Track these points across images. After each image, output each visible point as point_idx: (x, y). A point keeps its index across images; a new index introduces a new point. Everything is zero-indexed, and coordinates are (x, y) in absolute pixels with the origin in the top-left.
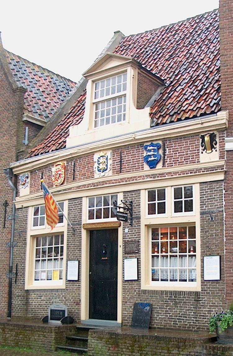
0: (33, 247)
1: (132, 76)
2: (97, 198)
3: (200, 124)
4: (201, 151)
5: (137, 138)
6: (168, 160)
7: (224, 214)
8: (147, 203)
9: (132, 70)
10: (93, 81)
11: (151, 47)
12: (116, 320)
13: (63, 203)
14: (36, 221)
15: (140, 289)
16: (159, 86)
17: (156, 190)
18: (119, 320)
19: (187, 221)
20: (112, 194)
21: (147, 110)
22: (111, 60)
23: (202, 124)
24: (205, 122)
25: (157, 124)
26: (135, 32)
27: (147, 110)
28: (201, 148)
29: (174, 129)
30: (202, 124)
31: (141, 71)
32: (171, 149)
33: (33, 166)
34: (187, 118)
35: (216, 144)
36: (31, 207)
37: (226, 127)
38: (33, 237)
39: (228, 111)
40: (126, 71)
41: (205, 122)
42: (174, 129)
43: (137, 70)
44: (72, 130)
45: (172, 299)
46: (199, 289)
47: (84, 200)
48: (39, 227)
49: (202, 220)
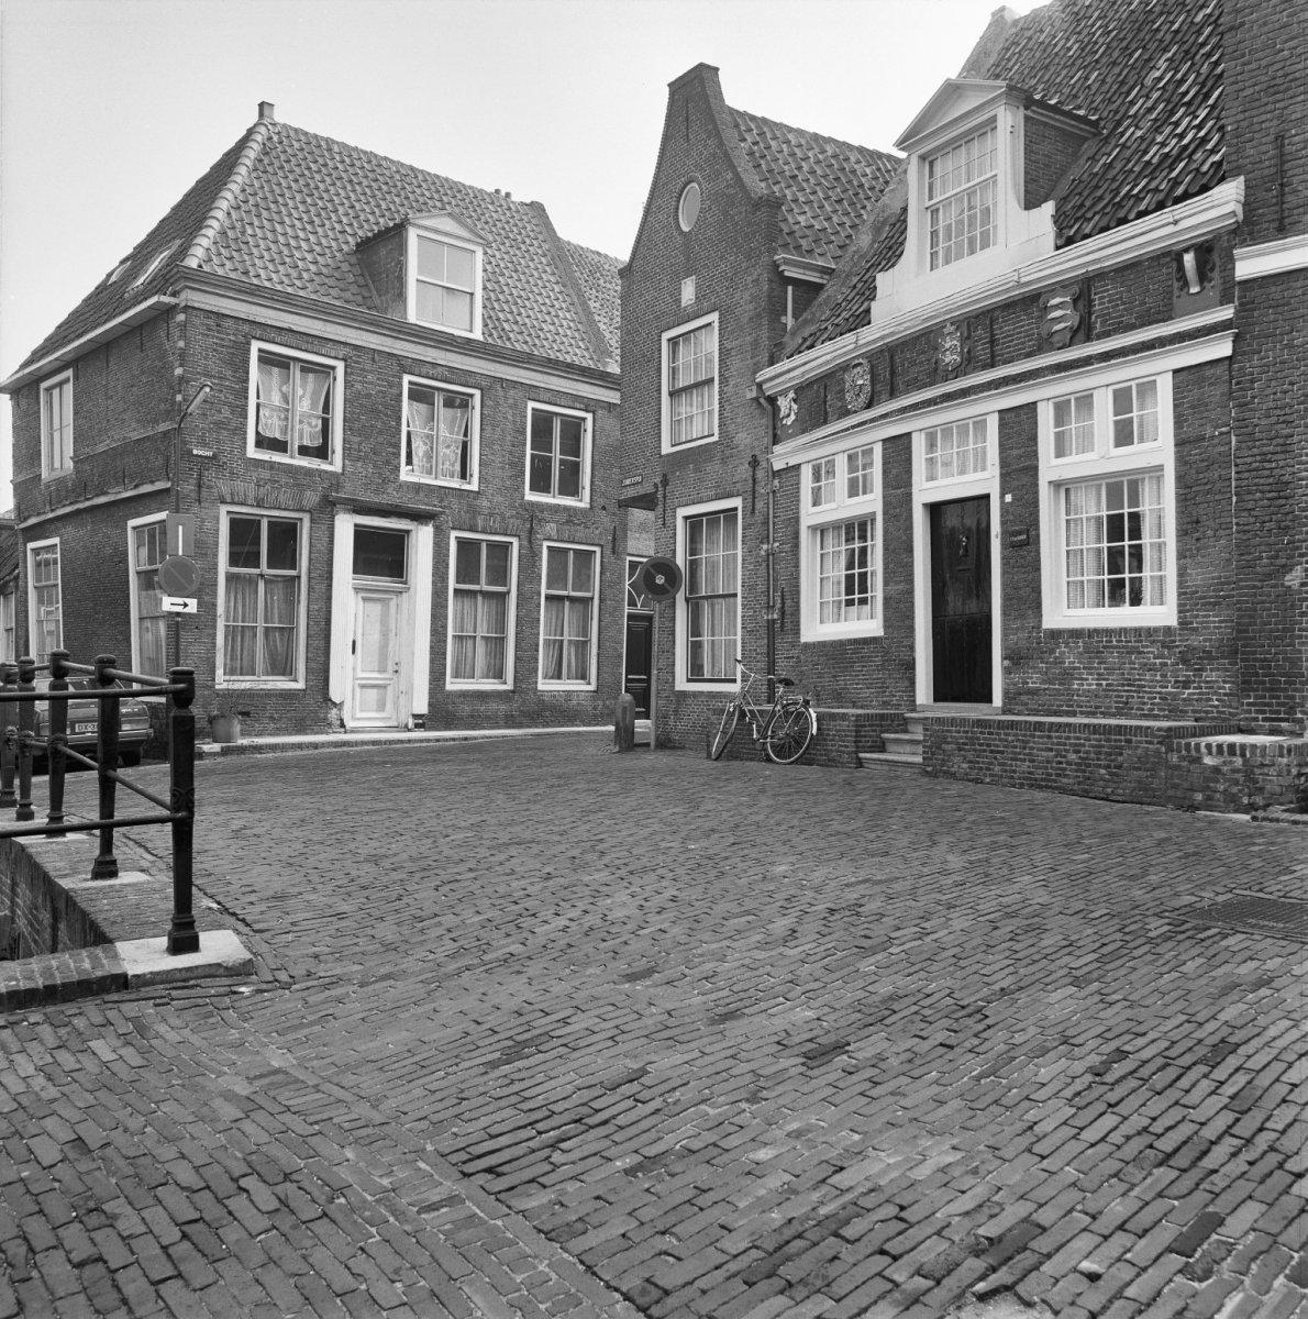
0: (814, 550)
1: (1010, 129)
2: (958, 427)
3: (1169, 224)
4: (1176, 293)
5: (1023, 280)
6: (1098, 325)
7: (1233, 438)
8: (1112, 418)
9: (1009, 114)
10: (923, 158)
11: (1079, 33)
12: (990, 701)
13: (985, 420)
14: (1060, 439)
15: (1039, 626)
16: (1086, 139)
17: (1072, 398)
18: (998, 699)
19: (1145, 465)
20: (1141, 381)
21: (1049, 208)
22: (959, 97)
23: (1176, 222)
24: (1185, 218)
25: (1070, 241)
26: (575, 241)
27: (1049, 208)
28: (1176, 285)
29: (1133, 237)
30: (1176, 222)
31: (1034, 112)
32: (1104, 297)
33: (803, 374)
34: (1141, 215)
35: (1212, 270)
36: (1044, 403)
37: (1237, 222)
38: (813, 528)
39: (1242, 178)
40: (994, 119)
41: (1185, 218)
42: (1133, 237)
43: (1021, 112)
44: (883, 280)
45: (1112, 647)
46: (1173, 621)
47: (1041, 407)
48: (861, 498)
49: (1181, 460)
